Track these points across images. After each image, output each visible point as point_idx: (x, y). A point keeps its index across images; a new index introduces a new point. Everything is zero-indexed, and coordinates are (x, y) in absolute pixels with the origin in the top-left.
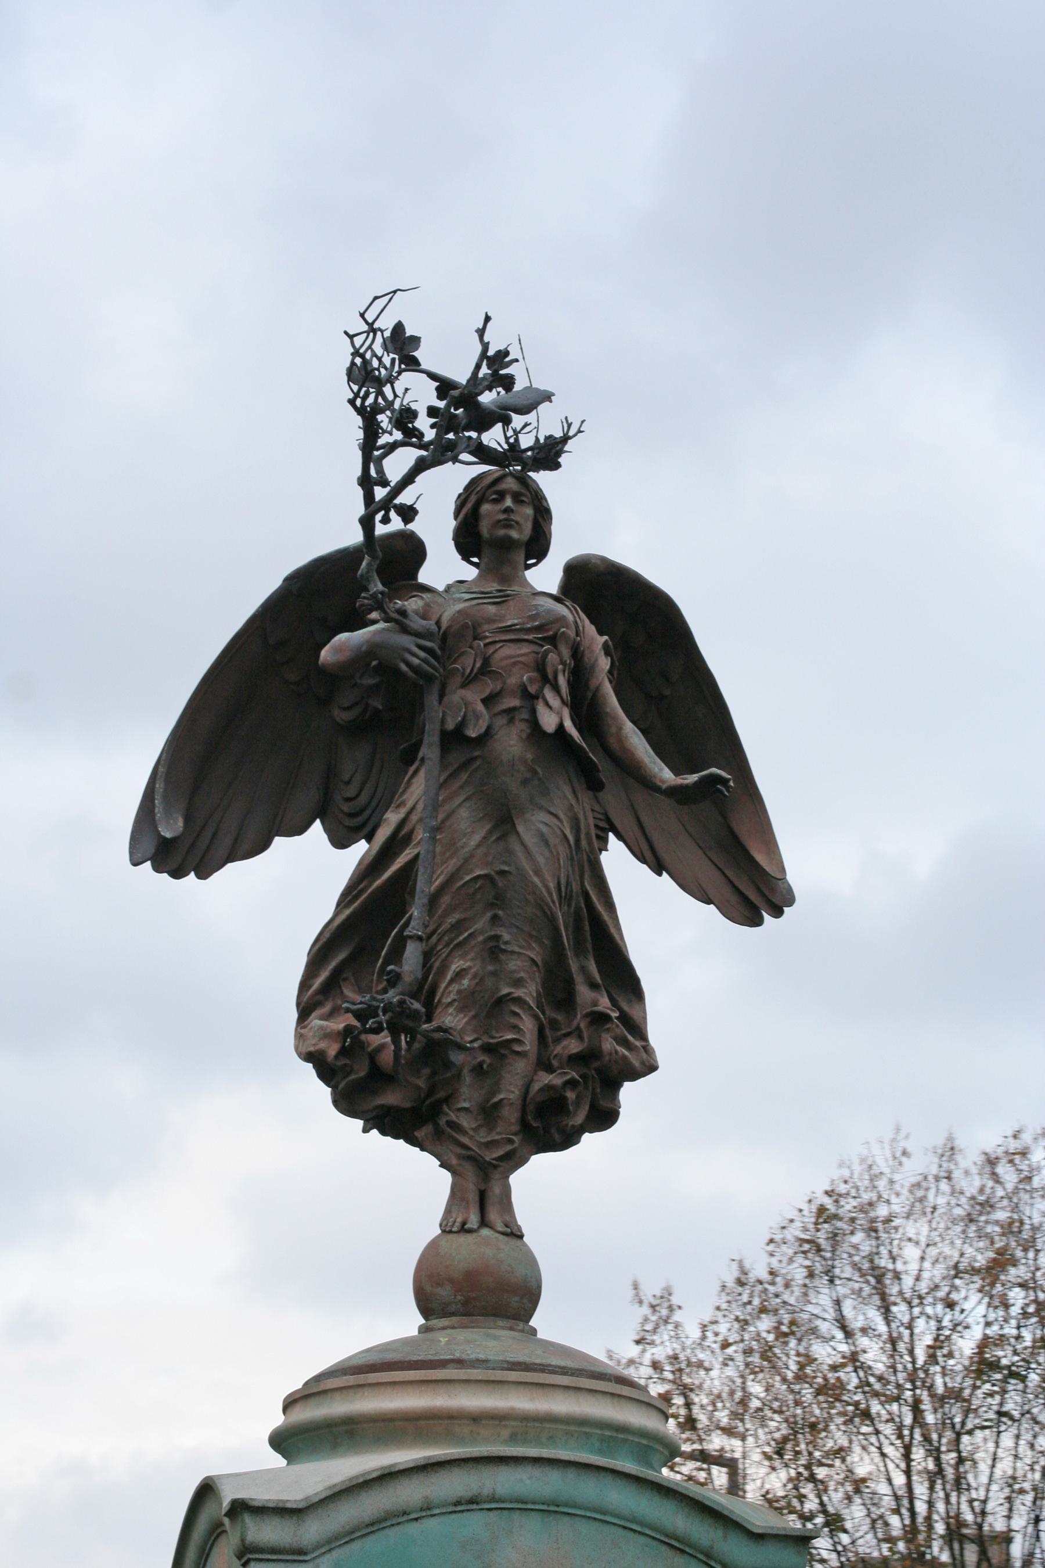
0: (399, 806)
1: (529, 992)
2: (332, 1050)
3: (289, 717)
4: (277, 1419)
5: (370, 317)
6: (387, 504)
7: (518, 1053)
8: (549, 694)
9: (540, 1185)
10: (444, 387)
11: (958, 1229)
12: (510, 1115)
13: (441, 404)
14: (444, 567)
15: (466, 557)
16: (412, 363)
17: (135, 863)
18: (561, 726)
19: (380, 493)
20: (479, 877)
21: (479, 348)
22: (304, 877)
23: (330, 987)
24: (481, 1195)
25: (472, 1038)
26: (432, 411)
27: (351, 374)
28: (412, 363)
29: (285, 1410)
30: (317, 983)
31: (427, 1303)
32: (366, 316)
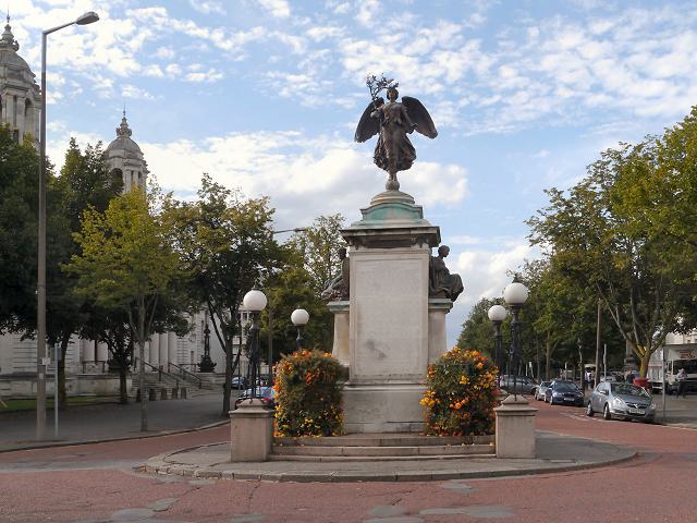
9: (400, 175)
14: (387, 101)
24: (393, 176)
25: (396, 157)
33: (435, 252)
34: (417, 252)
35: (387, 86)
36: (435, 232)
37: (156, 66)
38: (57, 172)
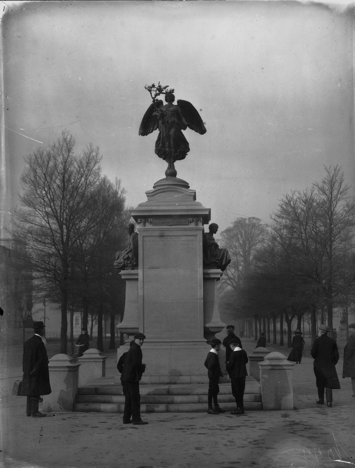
4: (153, 186)
9: (178, 164)
11: (25, 235)
17: (19, 394)
22: (155, 134)
25: (173, 149)
33: (207, 230)
34: (191, 230)
35: (164, 91)
36: (207, 213)
37: (70, 225)
38: (119, 273)
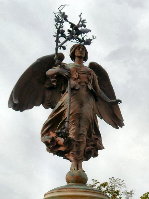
0: (61, 101)
1: (85, 133)
2: (49, 141)
3: (36, 85)
5: (60, 9)
6: (61, 46)
7: (83, 143)
8: (90, 83)
9: (85, 165)
10: (72, 25)
12: (82, 153)
13: (71, 29)
14: (67, 60)
15: (72, 59)
16: (66, 20)
18: (92, 89)
19: (59, 44)
20: (77, 113)
21: (80, 19)
23: (47, 131)
25: (73, 139)
26: (69, 31)
27: (55, 20)
28: (66, 20)
29: (44, 196)
30: (45, 130)
31: (68, 182)
32: (59, 9)
